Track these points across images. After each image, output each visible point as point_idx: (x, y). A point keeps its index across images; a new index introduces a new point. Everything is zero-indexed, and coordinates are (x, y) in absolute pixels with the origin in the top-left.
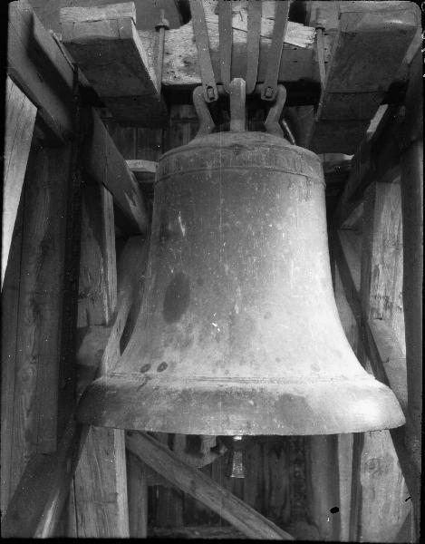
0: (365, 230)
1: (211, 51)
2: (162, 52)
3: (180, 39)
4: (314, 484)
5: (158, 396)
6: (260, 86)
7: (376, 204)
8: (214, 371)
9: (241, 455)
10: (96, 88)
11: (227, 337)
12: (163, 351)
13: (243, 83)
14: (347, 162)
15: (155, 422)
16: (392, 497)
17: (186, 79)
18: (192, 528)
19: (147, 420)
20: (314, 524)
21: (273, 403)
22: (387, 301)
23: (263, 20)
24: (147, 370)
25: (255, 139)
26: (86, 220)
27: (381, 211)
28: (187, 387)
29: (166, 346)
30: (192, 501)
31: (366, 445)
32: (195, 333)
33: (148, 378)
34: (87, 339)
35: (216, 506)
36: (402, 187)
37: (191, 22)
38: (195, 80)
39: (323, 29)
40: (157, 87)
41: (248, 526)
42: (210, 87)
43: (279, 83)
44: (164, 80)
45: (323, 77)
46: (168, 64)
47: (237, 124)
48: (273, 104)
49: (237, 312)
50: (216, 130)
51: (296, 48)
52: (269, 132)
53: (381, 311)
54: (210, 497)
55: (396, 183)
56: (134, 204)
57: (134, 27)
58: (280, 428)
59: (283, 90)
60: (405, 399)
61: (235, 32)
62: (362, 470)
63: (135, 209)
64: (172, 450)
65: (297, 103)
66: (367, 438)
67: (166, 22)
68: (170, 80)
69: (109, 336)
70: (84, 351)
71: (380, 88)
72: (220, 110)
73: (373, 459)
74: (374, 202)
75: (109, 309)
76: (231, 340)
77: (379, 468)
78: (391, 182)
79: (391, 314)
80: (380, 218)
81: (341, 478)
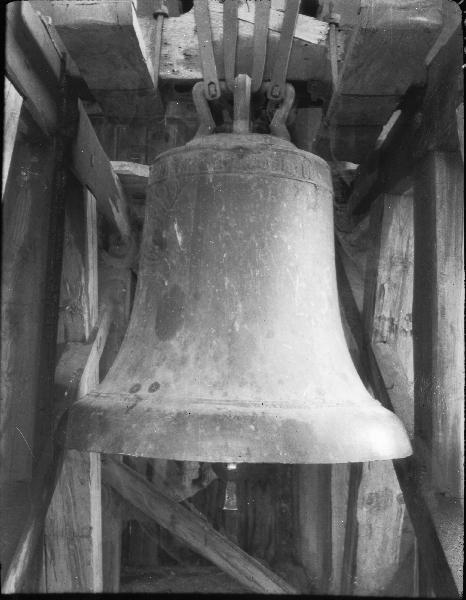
0: (373, 240)
1: (214, 44)
2: (160, 43)
3: (181, 30)
4: (302, 522)
5: (149, 419)
6: (268, 84)
7: (384, 219)
8: (211, 393)
9: (235, 486)
10: (86, 78)
11: (227, 356)
12: (154, 371)
13: (248, 80)
14: (350, 172)
15: (146, 446)
16: (390, 535)
17: (186, 74)
18: (167, 568)
19: (137, 444)
20: (301, 565)
21: (275, 428)
22: (392, 324)
23: (272, 11)
24: (137, 390)
25: (263, 142)
26: (67, 226)
27: (390, 224)
28: (182, 410)
29: (158, 365)
30: (169, 537)
31: (364, 479)
32: (191, 352)
33: (139, 399)
34: (65, 356)
35: (197, 544)
36: (416, 201)
37: (192, 11)
38: (196, 74)
39: (337, 25)
40: (154, 80)
41: (232, 565)
42: (212, 83)
43: (288, 81)
44: (162, 73)
45: (336, 77)
46: (166, 56)
47: (241, 125)
48: (277, 105)
49: (237, 330)
50: (215, 131)
51: (307, 44)
52: (275, 135)
53: (386, 334)
54: (191, 533)
55: (406, 196)
56: (118, 211)
57: (134, 12)
58: (283, 457)
59: (291, 89)
60: (412, 427)
61: (241, 23)
62: (359, 505)
63: (119, 217)
64: (150, 480)
65: (293, 100)
66: (366, 470)
67: (165, 9)
68: (167, 73)
69: (88, 354)
70: (61, 370)
71: (397, 91)
72: (221, 111)
73: (371, 494)
74: (382, 215)
75: (90, 325)
76: (231, 361)
77: (378, 503)
78: (401, 195)
79: (396, 338)
80: (387, 234)
81: (334, 514)
